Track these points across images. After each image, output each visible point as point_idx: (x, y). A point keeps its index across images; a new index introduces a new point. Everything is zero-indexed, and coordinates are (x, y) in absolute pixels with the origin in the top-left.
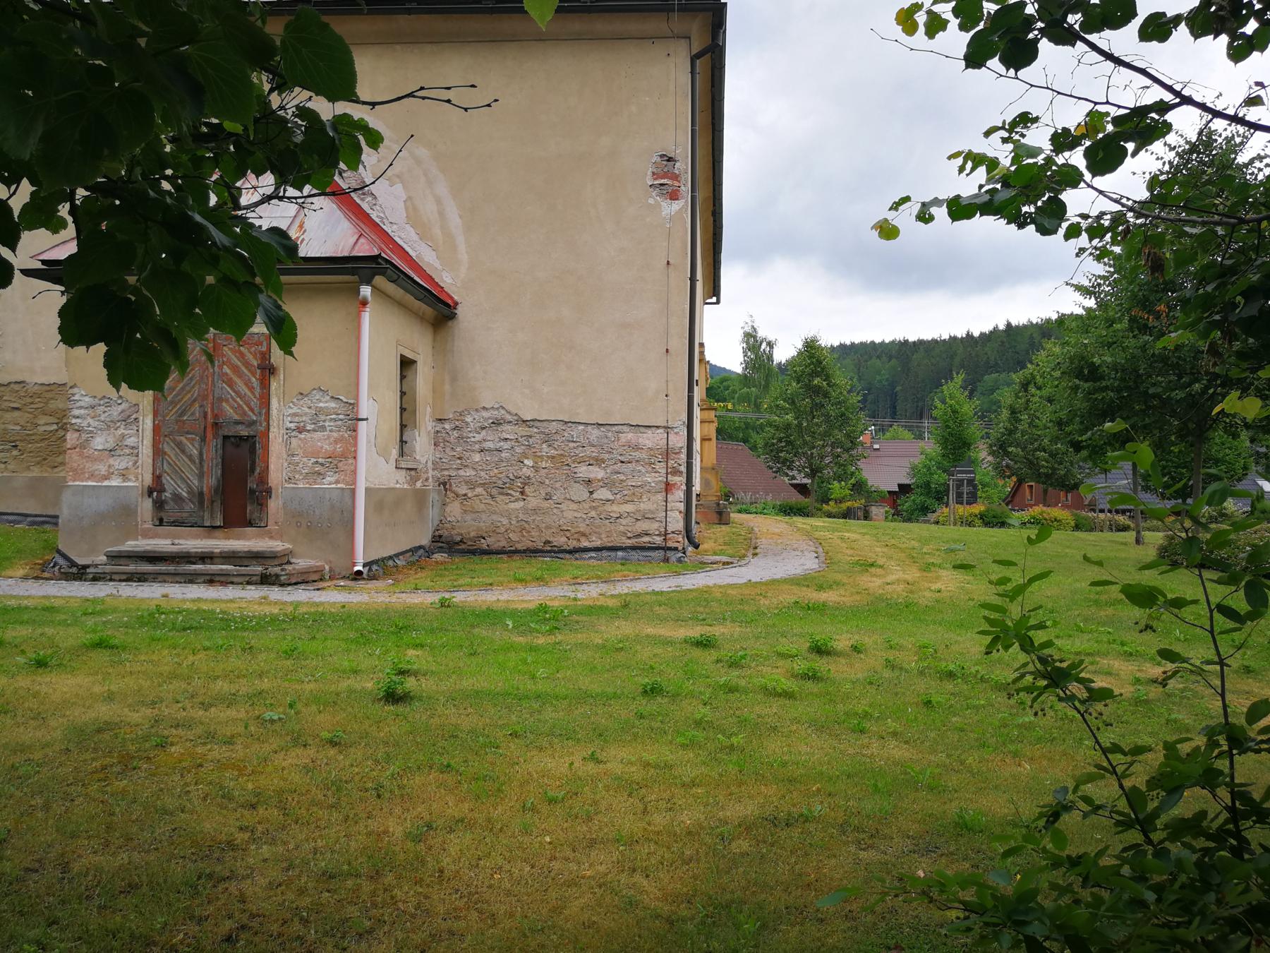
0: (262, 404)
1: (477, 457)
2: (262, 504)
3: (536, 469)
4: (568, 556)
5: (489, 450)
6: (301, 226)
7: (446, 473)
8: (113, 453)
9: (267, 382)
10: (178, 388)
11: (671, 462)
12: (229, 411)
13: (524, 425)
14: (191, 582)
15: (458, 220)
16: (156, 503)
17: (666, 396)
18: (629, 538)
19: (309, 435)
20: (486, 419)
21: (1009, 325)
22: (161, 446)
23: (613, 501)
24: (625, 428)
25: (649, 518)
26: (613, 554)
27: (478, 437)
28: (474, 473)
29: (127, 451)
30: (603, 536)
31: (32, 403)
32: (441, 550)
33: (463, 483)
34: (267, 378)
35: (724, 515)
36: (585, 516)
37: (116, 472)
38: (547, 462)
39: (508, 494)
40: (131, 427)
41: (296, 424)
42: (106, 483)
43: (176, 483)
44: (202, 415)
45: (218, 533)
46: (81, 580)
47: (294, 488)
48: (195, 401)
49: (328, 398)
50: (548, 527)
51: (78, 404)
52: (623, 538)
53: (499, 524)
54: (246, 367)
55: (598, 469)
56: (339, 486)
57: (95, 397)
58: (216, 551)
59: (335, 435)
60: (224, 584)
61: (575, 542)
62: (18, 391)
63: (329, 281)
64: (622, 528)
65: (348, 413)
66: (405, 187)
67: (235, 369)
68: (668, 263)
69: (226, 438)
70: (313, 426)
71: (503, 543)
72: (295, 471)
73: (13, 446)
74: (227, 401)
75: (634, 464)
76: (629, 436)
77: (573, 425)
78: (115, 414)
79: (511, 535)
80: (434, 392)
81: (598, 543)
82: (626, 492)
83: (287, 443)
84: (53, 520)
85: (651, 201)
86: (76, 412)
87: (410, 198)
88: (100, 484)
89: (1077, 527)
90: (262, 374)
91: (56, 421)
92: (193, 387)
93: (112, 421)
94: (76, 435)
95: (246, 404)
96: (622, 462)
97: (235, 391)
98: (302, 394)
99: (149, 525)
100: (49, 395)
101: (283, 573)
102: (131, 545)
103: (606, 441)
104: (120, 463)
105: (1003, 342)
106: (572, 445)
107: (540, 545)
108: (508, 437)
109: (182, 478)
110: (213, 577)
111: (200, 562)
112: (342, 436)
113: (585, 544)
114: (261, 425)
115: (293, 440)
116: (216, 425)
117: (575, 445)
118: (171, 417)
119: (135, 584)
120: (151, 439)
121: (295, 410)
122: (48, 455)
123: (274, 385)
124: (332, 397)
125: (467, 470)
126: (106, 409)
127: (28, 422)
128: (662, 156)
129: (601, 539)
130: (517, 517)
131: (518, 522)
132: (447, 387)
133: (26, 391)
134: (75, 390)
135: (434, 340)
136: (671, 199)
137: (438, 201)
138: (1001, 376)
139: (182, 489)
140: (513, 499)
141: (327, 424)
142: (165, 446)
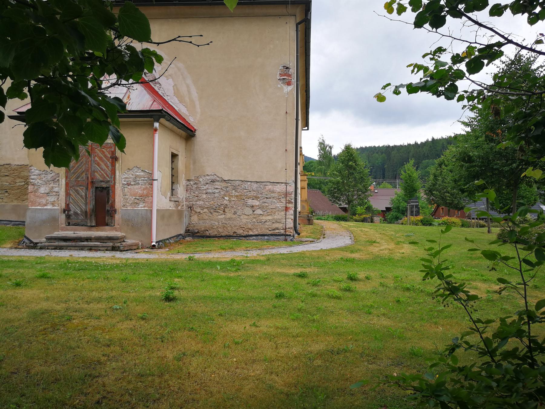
0: (112, 173)
1: (204, 196)
2: (112, 216)
3: (230, 201)
4: (244, 238)
5: (210, 193)
6: (129, 97)
7: (191, 203)
8: (48, 194)
10: (76, 167)
11: (288, 198)
12: (98, 176)
14: (82, 250)
17: (286, 170)
18: (270, 231)
19: (132, 187)
20: (208, 180)
21: (433, 139)
22: (69, 192)
23: (263, 215)
24: (268, 183)
26: (263, 237)
27: (205, 187)
29: (54, 194)
30: (259, 230)
31: (14, 173)
32: (189, 236)
33: (199, 207)
34: (114, 162)
35: (311, 221)
36: (251, 221)
37: (50, 203)
38: (234, 198)
39: (218, 212)
42: (45, 207)
43: (75, 207)
44: (86, 178)
46: (35, 249)
48: (83, 172)
49: (140, 171)
50: (235, 226)
54: (105, 158)
55: (256, 201)
56: (145, 208)
57: (40, 170)
59: (144, 186)
60: (96, 250)
61: (246, 232)
64: (267, 226)
65: (149, 177)
67: (101, 158)
68: (286, 112)
69: (97, 188)
70: (134, 183)
71: (216, 233)
72: (126, 202)
73: (6, 192)
74: (97, 172)
76: (270, 187)
79: (219, 229)
80: (186, 168)
81: (256, 233)
82: (268, 211)
83: (123, 190)
85: (279, 86)
86: (32, 177)
87: (175, 85)
88: (43, 208)
89: (463, 226)
91: (24, 181)
92: (83, 166)
93: (48, 181)
94: (33, 187)
95: (105, 173)
96: (267, 198)
97: (100, 168)
99: (64, 226)
100: (21, 170)
101: (122, 246)
104: (51, 199)
105: (430, 146)
106: (245, 191)
107: (231, 234)
108: (218, 187)
109: (78, 205)
110: (91, 248)
111: (86, 241)
112: (146, 187)
113: (251, 233)
114: (112, 182)
115: (126, 189)
116: (92, 182)
117: (246, 191)
118: (73, 179)
119: (58, 251)
121: (126, 176)
122: (20, 195)
123: (117, 165)
124: (142, 170)
125: (200, 202)
126: (45, 176)
127: (12, 181)
130: (222, 222)
132: (192, 166)
133: (11, 168)
134: (32, 168)
135: (186, 146)
137: (188, 86)
138: (430, 161)
139: (78, 210)
140: (220, 214)
142: (71, 191)
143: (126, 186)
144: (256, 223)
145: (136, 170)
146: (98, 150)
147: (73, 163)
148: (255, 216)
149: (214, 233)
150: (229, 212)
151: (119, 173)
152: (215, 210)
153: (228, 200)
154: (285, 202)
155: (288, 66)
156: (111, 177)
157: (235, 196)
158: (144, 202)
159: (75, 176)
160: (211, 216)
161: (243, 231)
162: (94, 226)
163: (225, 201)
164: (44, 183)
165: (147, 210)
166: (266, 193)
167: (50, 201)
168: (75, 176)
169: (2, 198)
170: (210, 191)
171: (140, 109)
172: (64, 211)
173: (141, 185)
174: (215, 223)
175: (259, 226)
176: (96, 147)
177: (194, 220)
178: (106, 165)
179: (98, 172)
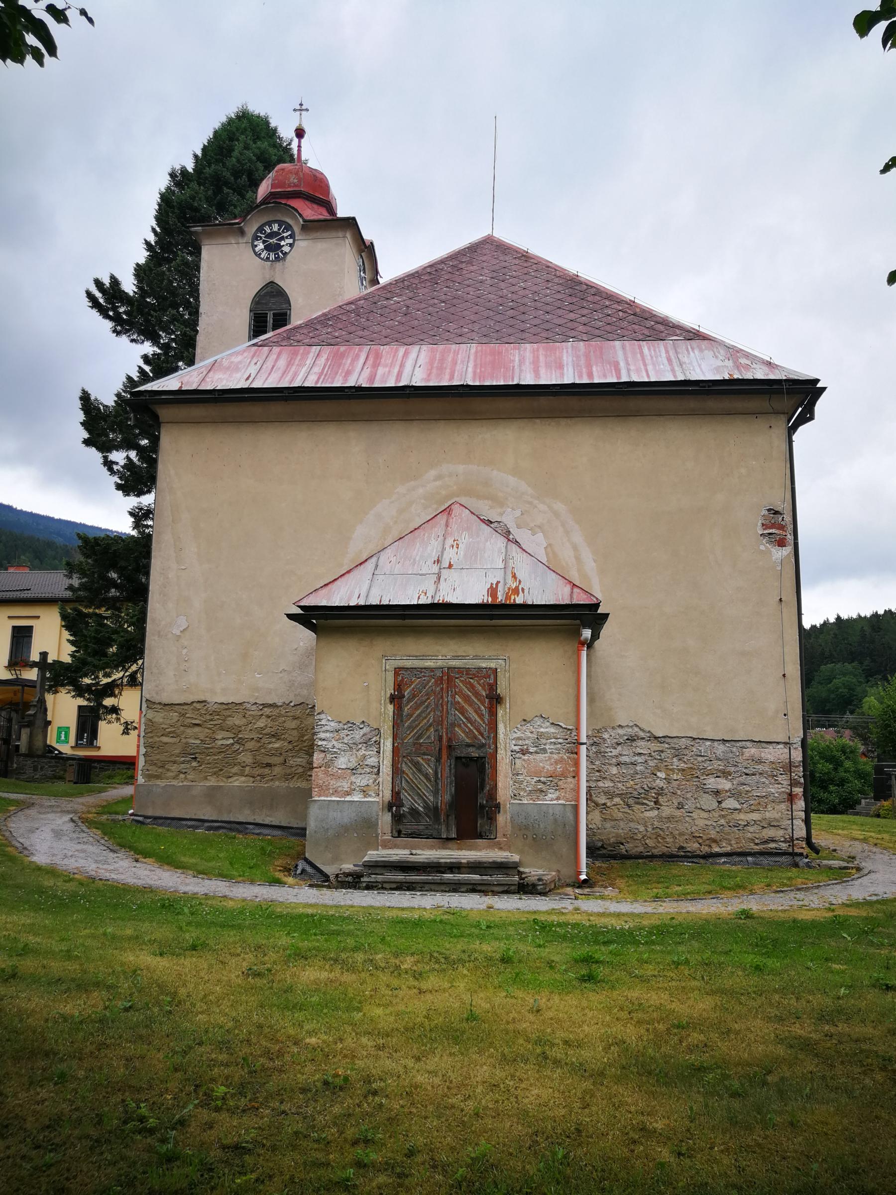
1: (614, 770)
2: (492, 819)
3: (668, 780)
4: (702, 861)
5: (625, 764)
8: (354, 771)
9: (495, 709)
10: (415, 715)
13: (656, 741)
14: (455, 891)
15: (593, 564)
16: (395, 817)
17: (785, 715)
19: (531, 757)
20: (621, 736)
21: (839, 618)
22: (399, 766)
23: (740, 810)
24: (748, 744)
25: (774, 826)
27: (615, 752)
28: (612, 785)
29: (368, 770)
30: (733, 842)
31: (212, 720)
33: (602, 794)
34: (495, 706)
37: (357, 789)
38: (677, 774)
39: (643, 804)
40: (371, 749)
41: (520, 747)
42: (348, 798)
43: (412, 798)
44: (437, 738)
45: (450, 844)
46: (355, 888)
47: (520, 804)
48: (430, 725)
49: (548, 724)
50: (681, 834)
51: (324, 729)
52: (751, 844)
53: (637, 831)
54: (476, 697)
55: (725, 781)
56: (560, 802)
57: (340, 722)
58: (463, 861)
59: (555, 756)
60: (485, 893)
61: (707, 848)
62: (199, 709)
63: (548, 624)
64: (749, 835)
65: (567, 737)
66: (545, 536)
67: (466, 699)
68: (781, 600)
70: (535, 749)
71: (641, 849)
72: (519, 788)
73: (193, 758)
75: (757, 776)
76: (752, 751)
77: (701, 741)
78: (357, 737)
79: (647, 841)
82: (752, 802)
83: (513, 763)
84: (301, 832)
86: (322, 735)
87: (550, 545)
88: (343, 799)
90: (490, 702)
91: (233, 736)
92: (429, 714)
93: (354, 744)
94: (322, 755)
95: (476, 729)
96: (747, 774)
97: (466, 718)
98: (525, 720)
99: (388, 837)
100: (228, 713)
101: (541, 883)
102: (373, 855)
103: (731, 755)
104: (361, 781)
105: (835, 635)
106: (700, 759)
107: (674, 850)
109: (419, 795)
111: (448, 871)
112: (562, 758)
113: (716, 849)
114: (490, 748)
118: (409, 740)
119: (418, 893)
120: (391, 760)
121: (519, 734)
122: (224, 766)
123: (500, 713)
124: (552, 724)
125: (606, 782)
126: (349, 733)
127: (207, 737)
128: (769, 510)
129: (731, 845)
131: (653, 829)
133: (206, 710)
134: (322, 716)
136: (779, 546)
137: (575, 548)
138: (838, 666)
139: (419, 805)
140: (648, 808)
141: (547, 747)
142: (404, 765)
143: (518, 755)
144: (727, 829)
145: (539, 721)
146: (461, 681)
147: (409, 707)
148: (723, 813)
149: (636, 849)
150: (666, 804)
151: (505, 729)
152: (637, 800)
153: (665, 779)
154: (786, 783)
155: (779, 509)
156: (488, 737)
157: (679, 770)
158: (557, 788)
159: (412, 734)
160: (629, 811)
161: (698, 846)
162: (454, 839)
163: (658, 781)
164: (346, 747)
165: (564, 805)
166: (745, 764)
167: (358, 784)
168: (412, 734)
169: (184, 771)
170: (624, 759)
171: (552, 603)
172: (390, 806)
173: (551, 753)
174: (639, 827)
175: (733, 835)
176: (457, 676)
177: (593, 822)
178: (477, 711)
179: (462, 725)
